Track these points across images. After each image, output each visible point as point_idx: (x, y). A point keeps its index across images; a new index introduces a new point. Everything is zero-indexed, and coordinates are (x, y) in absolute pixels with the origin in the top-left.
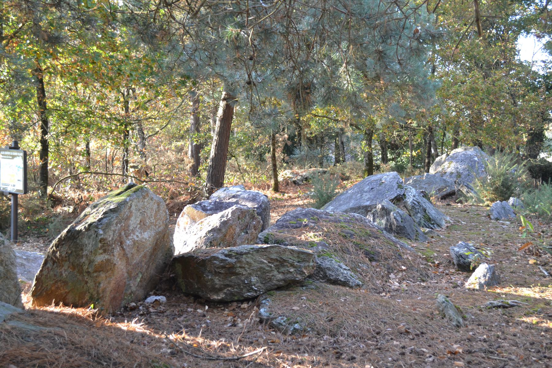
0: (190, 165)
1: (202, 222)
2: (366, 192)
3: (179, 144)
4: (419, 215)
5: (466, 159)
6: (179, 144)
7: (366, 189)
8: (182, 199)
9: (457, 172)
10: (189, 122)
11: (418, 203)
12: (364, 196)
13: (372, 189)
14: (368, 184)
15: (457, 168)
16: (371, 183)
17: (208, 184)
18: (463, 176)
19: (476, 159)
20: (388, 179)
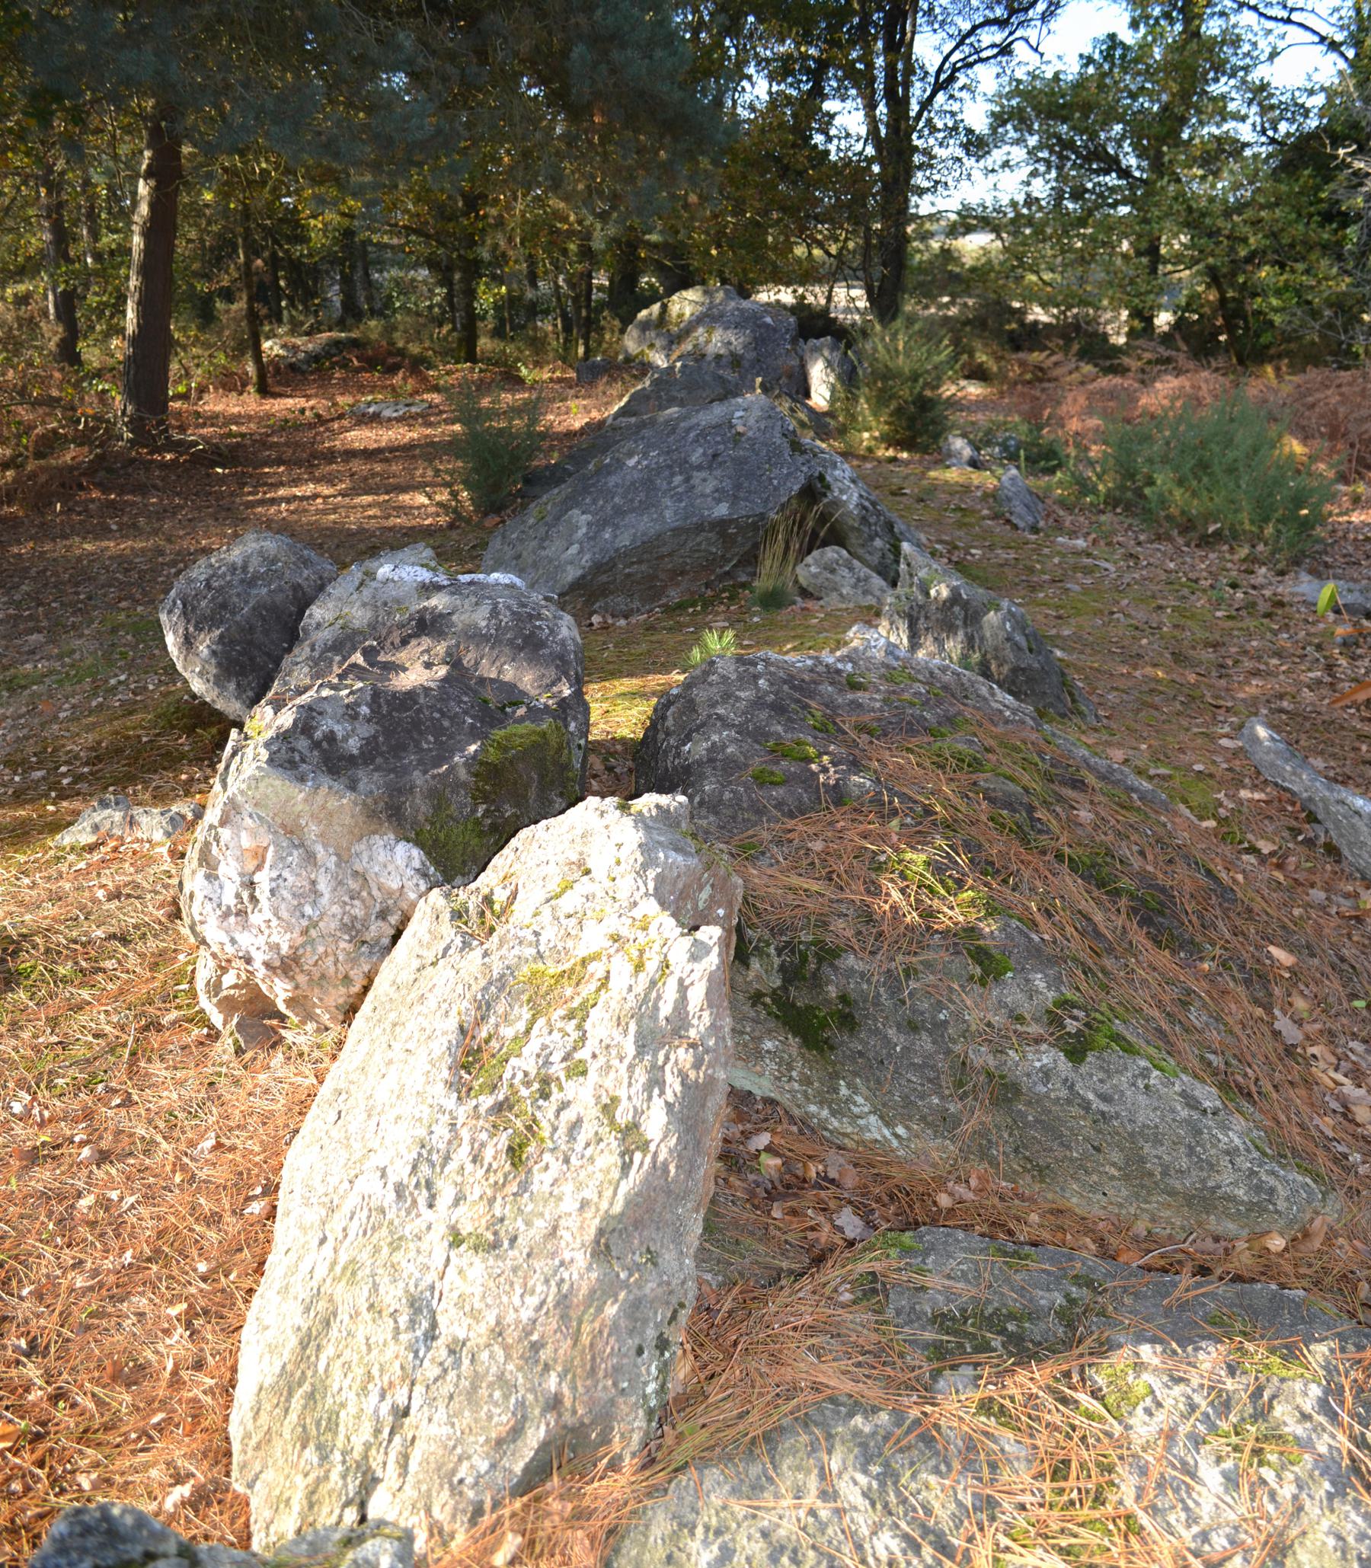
0: (56, 339)
1: (639, 967)
2: (699, 468)
3: (22, 288)
4: (878, 543)
5: (747, 320)
6: (22, 288)
7: (696, 457)
8: (68, 458)
9: (732, 354)
10: (40, 239)
11: (874, 504)
12: (695, 481)
13: (715, 456)
14: (696, 441)
15: (730, 343)
16: (703, 434)
17: (129, 408)
18: (746, 364)
19: (768, 320)
20: (751, 422)
